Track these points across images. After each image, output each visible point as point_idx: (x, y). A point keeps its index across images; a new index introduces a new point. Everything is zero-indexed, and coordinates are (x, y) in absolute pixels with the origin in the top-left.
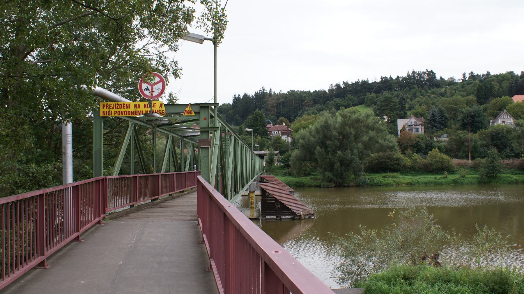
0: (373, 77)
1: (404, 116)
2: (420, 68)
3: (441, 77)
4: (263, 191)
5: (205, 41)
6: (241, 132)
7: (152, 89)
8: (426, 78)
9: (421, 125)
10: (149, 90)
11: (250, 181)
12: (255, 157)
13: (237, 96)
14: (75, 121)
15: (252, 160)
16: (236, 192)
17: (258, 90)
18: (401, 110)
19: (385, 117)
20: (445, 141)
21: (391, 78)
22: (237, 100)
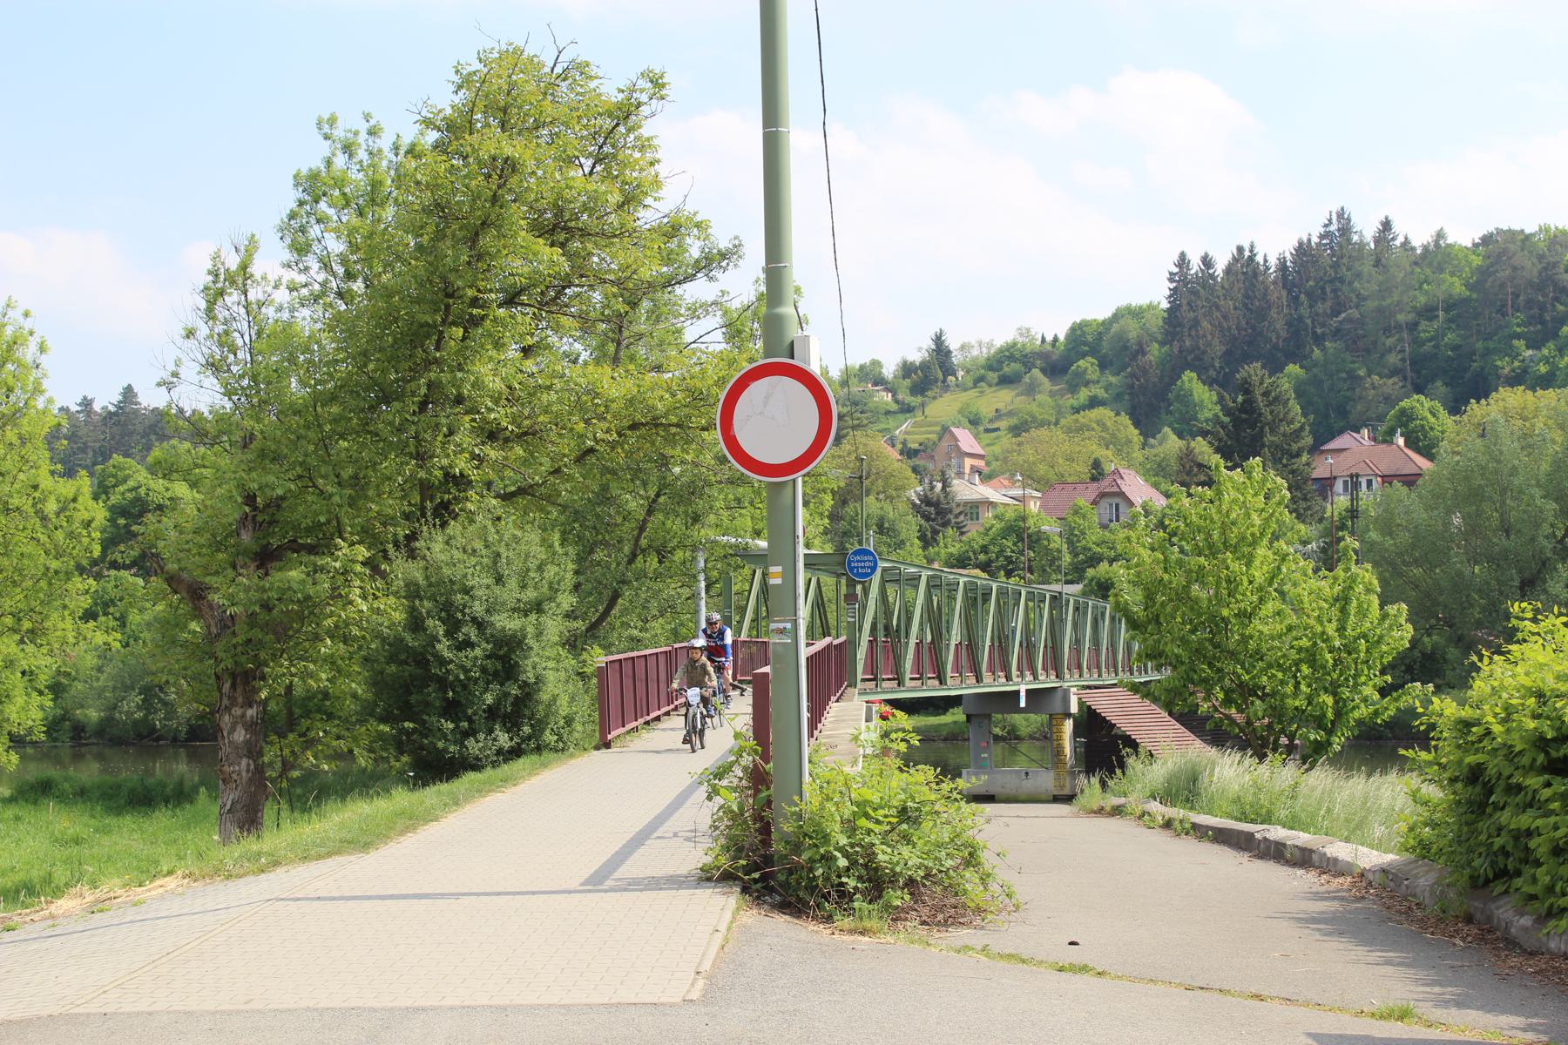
5: (575, 885)
13: (1195, 265)
17: (1311, 228)
22: (1191, 287)
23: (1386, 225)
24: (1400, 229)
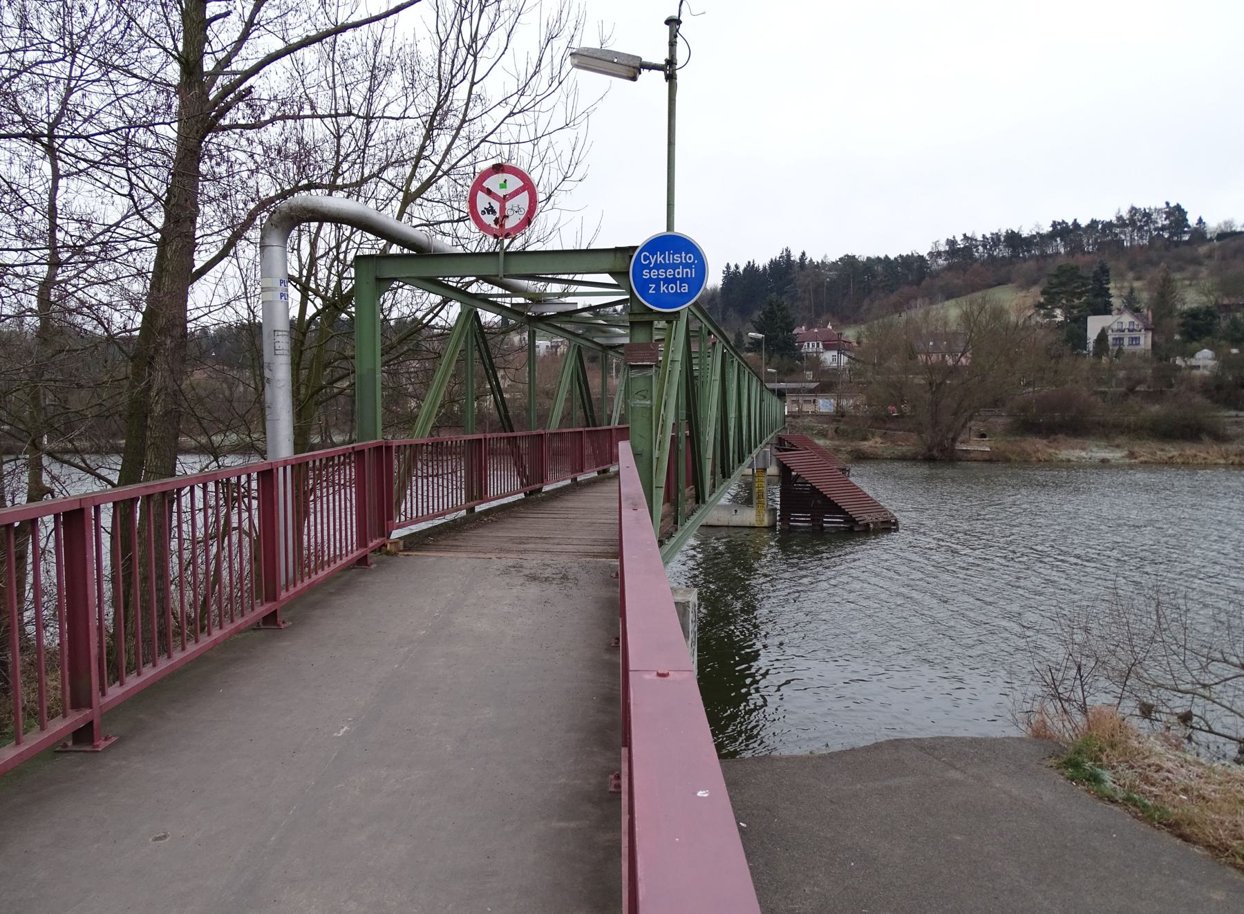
0: (1033, 220)
1: (1106, 310)
2: (1153, 200)
3: (1200, 220)
4: (785, 470)
5: (645, 72)
6: (738, 347)
7: (503, 208)
8: (1162, 221)
9: (1146, 329)
10: (494, 212)
11: (756, 446)
12: (767, 395)
13: (733, 268)
14: (1132, 222)
15: (761, 400)
16: (726, 474)
17: (776, 254)
18: (1096, 296)
19: (1058, 312)
20: (1205, 367)
21: (1075, 223)
23: (804, 254)
24: (808, 256)
